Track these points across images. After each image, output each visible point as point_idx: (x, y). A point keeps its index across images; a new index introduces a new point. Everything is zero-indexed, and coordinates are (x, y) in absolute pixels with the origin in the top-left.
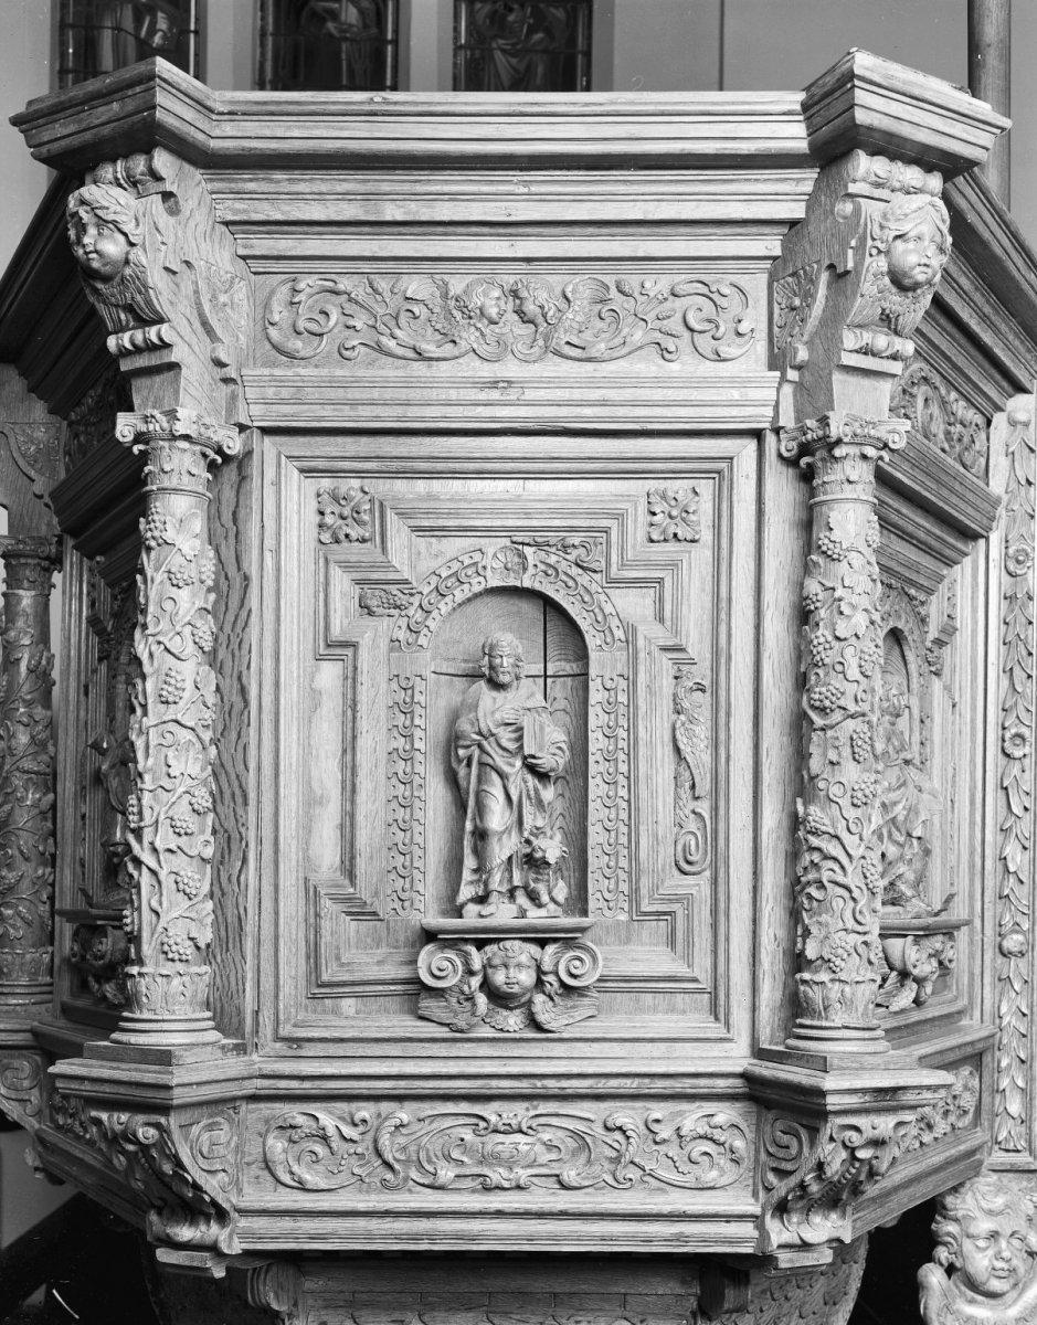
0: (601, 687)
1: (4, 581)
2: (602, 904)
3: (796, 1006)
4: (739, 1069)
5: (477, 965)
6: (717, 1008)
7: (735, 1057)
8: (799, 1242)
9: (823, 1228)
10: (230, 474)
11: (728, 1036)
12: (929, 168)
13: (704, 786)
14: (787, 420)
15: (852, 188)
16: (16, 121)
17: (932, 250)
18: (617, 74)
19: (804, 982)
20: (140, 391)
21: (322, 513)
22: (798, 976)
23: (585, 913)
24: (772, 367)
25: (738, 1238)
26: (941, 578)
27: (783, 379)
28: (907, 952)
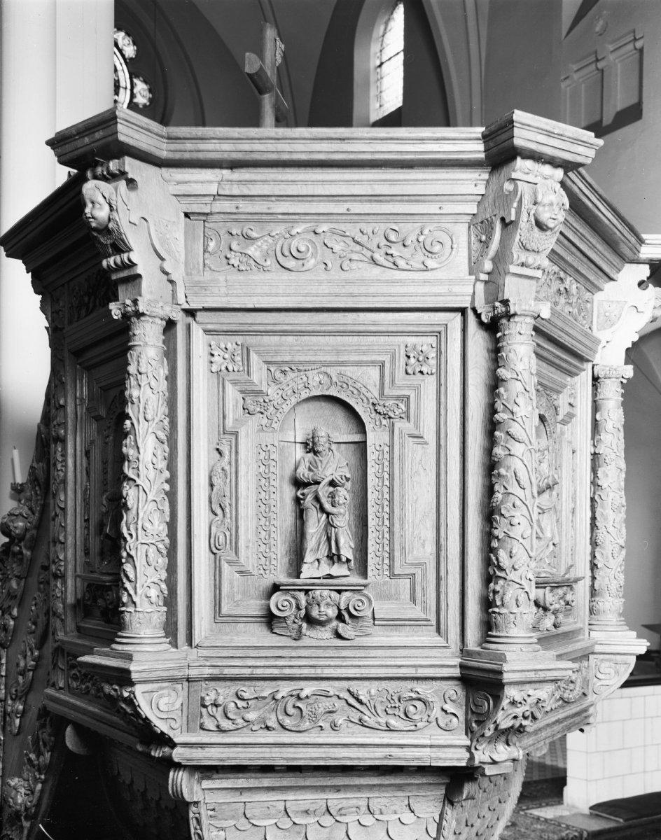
0: (374, 451)
5: (303, 603)
8: (490, 761)
9: (502, 752)
15: (514, 175)
16: (51, 143)
17: (556, 208)
18: (460, 118)
19: (495, 612)
20: (121, 290)
21: (409, 357)
22: (490, 610)
25: (457, 758)
26: (565, 386)
27: (477, 280)
28: (547, 596)
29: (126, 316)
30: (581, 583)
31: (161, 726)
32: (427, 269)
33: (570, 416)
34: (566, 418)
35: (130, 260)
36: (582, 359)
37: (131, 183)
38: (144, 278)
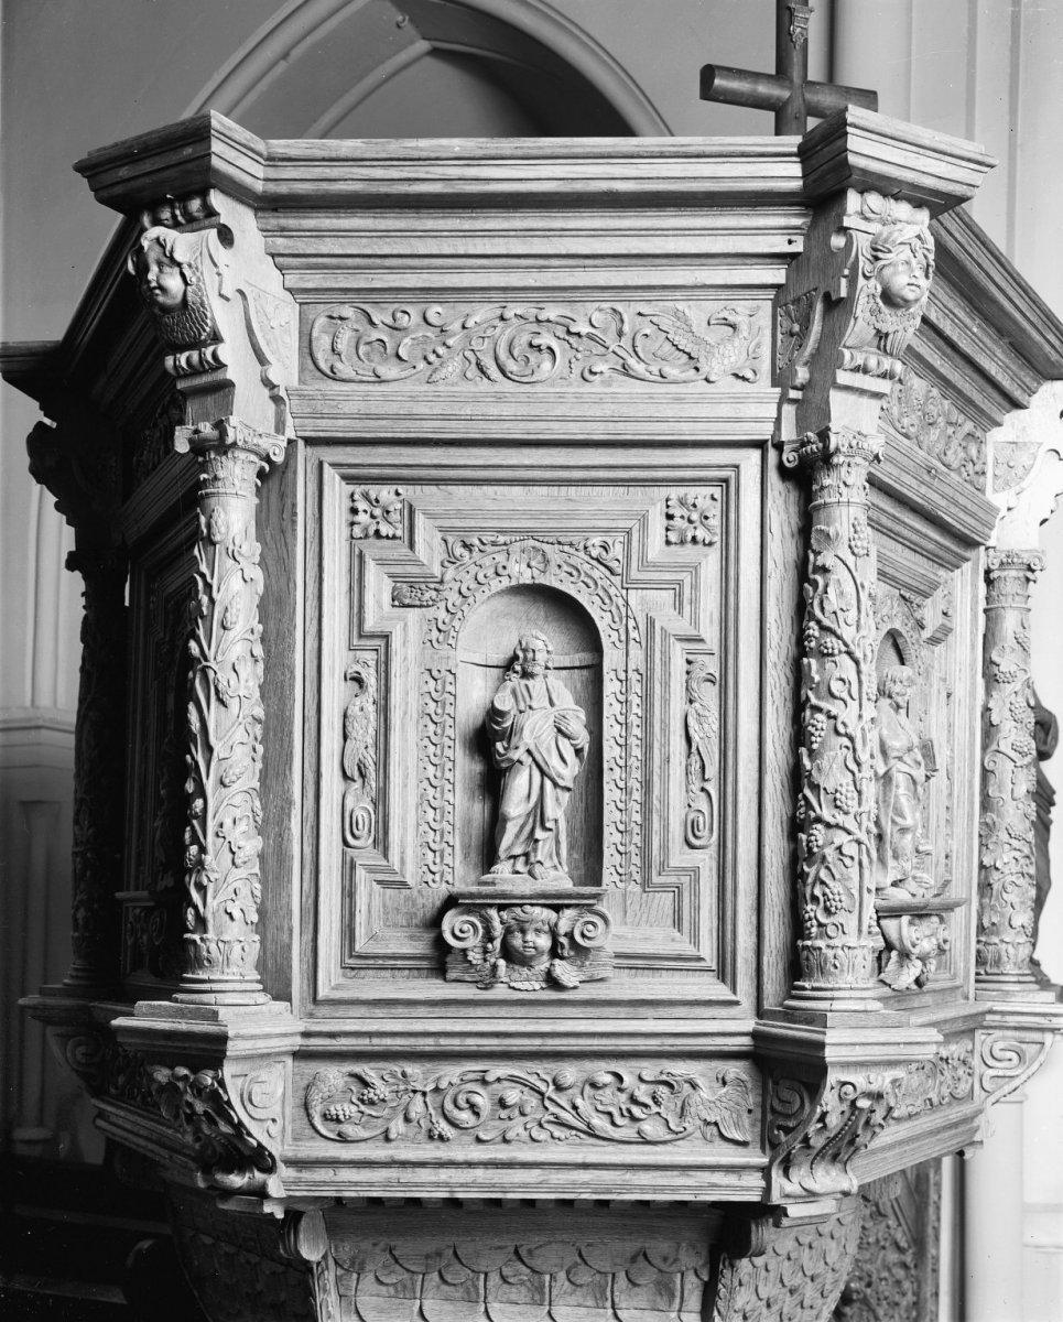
1: (84, 607)
2: (616, 878)
3: (798, 965)
4: (751, 1029)
6: (725, 970)
7: (741, 1023)
9: (826, 1179)
10: (274, 483)
11: (733, 998)
12: (918, 204)
13: (712, 771)
14: (788, 433)
23: (598, 883)
24: (774, 385)
25: (747, 1189)
26: (935, 586)
27: (783, 399)
29: (199, 447)
30: (960, 912)
31: (258, 1133)
32: (380, 380)
33: (946, 631)
34: (938, 635)
35: (214, 355)
36: (970, 543)
37: (226, 236)
38: (238, 390)
